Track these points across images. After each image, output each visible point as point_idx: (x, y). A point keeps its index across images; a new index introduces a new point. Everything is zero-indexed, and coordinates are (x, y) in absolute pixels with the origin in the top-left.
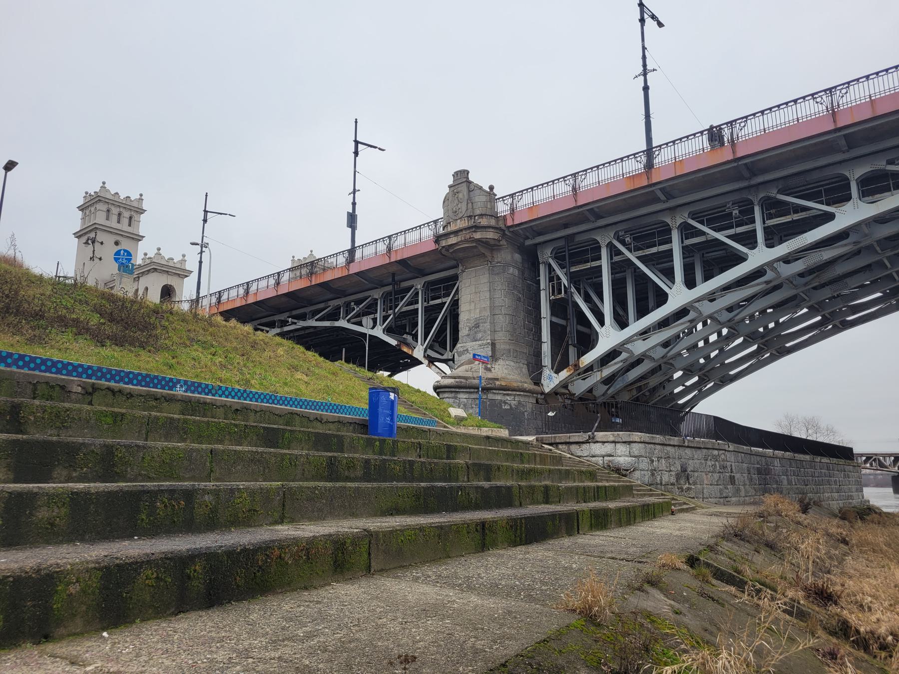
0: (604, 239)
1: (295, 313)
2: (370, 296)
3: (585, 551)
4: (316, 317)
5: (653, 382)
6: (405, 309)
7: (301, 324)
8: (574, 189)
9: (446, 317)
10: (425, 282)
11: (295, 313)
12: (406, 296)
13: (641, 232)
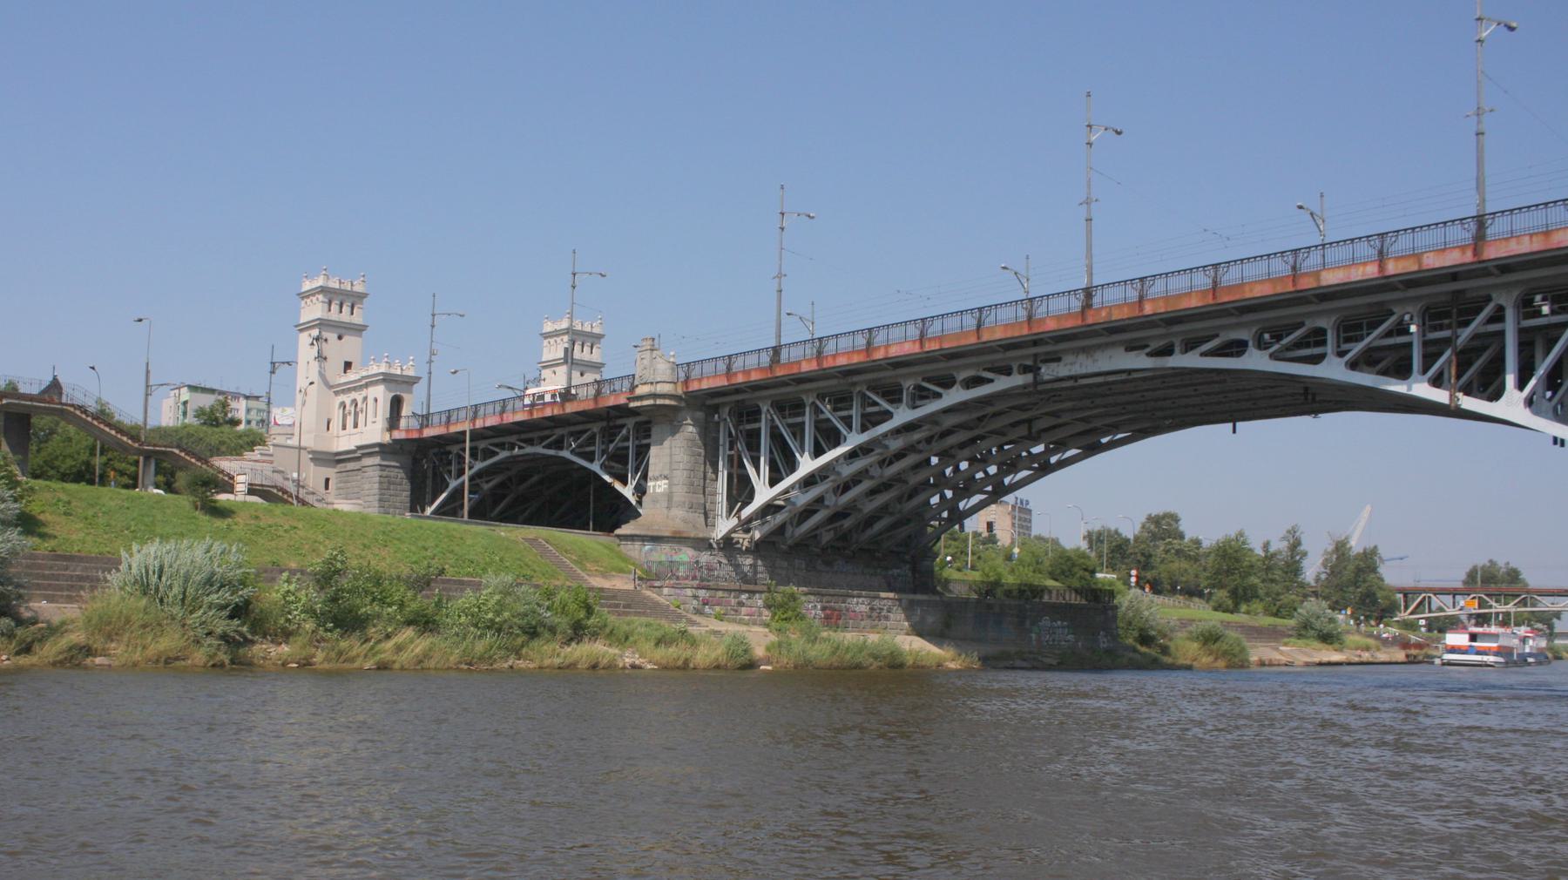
0: (809, 399)
1: (523, 436)
4: (544, 444)
5: (903, 532)
6: (1482, 330)
7: (529, 450)
8: (1215, 282)
9: (816, 438)
11: (523, 436)
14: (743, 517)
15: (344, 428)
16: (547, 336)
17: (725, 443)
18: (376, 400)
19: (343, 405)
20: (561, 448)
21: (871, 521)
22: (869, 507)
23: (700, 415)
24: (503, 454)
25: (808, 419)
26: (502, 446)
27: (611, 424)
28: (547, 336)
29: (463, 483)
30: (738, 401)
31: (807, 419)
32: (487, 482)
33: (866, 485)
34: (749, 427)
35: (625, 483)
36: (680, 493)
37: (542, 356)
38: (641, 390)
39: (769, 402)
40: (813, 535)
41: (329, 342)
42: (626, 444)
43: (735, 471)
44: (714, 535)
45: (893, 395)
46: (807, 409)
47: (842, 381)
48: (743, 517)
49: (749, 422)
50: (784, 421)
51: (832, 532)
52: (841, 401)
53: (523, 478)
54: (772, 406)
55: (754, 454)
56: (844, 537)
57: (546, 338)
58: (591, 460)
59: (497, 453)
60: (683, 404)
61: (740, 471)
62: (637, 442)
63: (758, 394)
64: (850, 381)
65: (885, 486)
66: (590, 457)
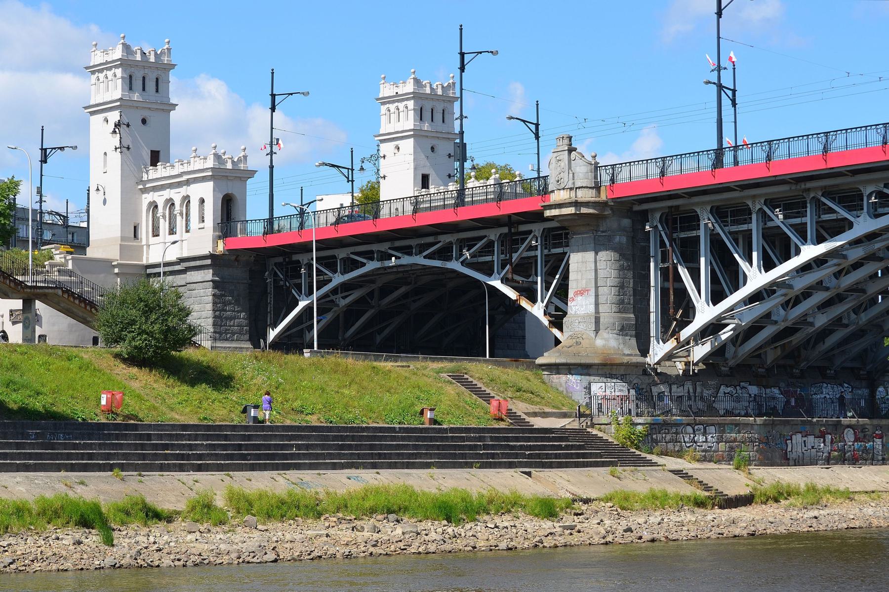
1: (398, 244)
2: (485, 236)
3: (768, 473)
4: (425, 254)
7: (406, 260)
10: (501, 234)
11: (398, 244)
12: (476, 244)
13: (737, 207)
14: (682, 339)
15: (156, 234)
16: (386, 101)
17: (656, 252)
18: (202, 201)
19: (154, 206)
20: (449, 259)
21: (825, 332)
22: (821, 320)
23: (626, 222)
24: (372, 266)
25: (754, 226)
26: (369, 255)
27: (513, 230)
28: (386, 101)
29: (312, 303)
30: (671, 207)
31: (754, 226)
32: (344, 298)
33: (819, 297)
34: (683, 235)
35: (533, 300)
36: (608, 314)
37: (379, 126)
38: (556, 197)
39: (709, 209)
40: (757, 353)
41: (131, 127)
42: (532, 253)
43: (670, 285)
44: (648, 360)
45: (853, 201)
46: (754, 217)
47: (793, 187)
48: (682, 339)
49: (683, 230)
50: (726, 229)
51: (779, 350)
52: (793, 207)
53: (385, 291)
54: (711, 212)
55: (691, 265)
56: (793, 355)
57: (383, 104)
58: (489, 273)
59: (363, 265)
60: (608, 212)
61: (677, 285)
62: (546, 252)
63: (696, 199)
64: (803, 187)
65: (839, 298)
66: (488, 270)
